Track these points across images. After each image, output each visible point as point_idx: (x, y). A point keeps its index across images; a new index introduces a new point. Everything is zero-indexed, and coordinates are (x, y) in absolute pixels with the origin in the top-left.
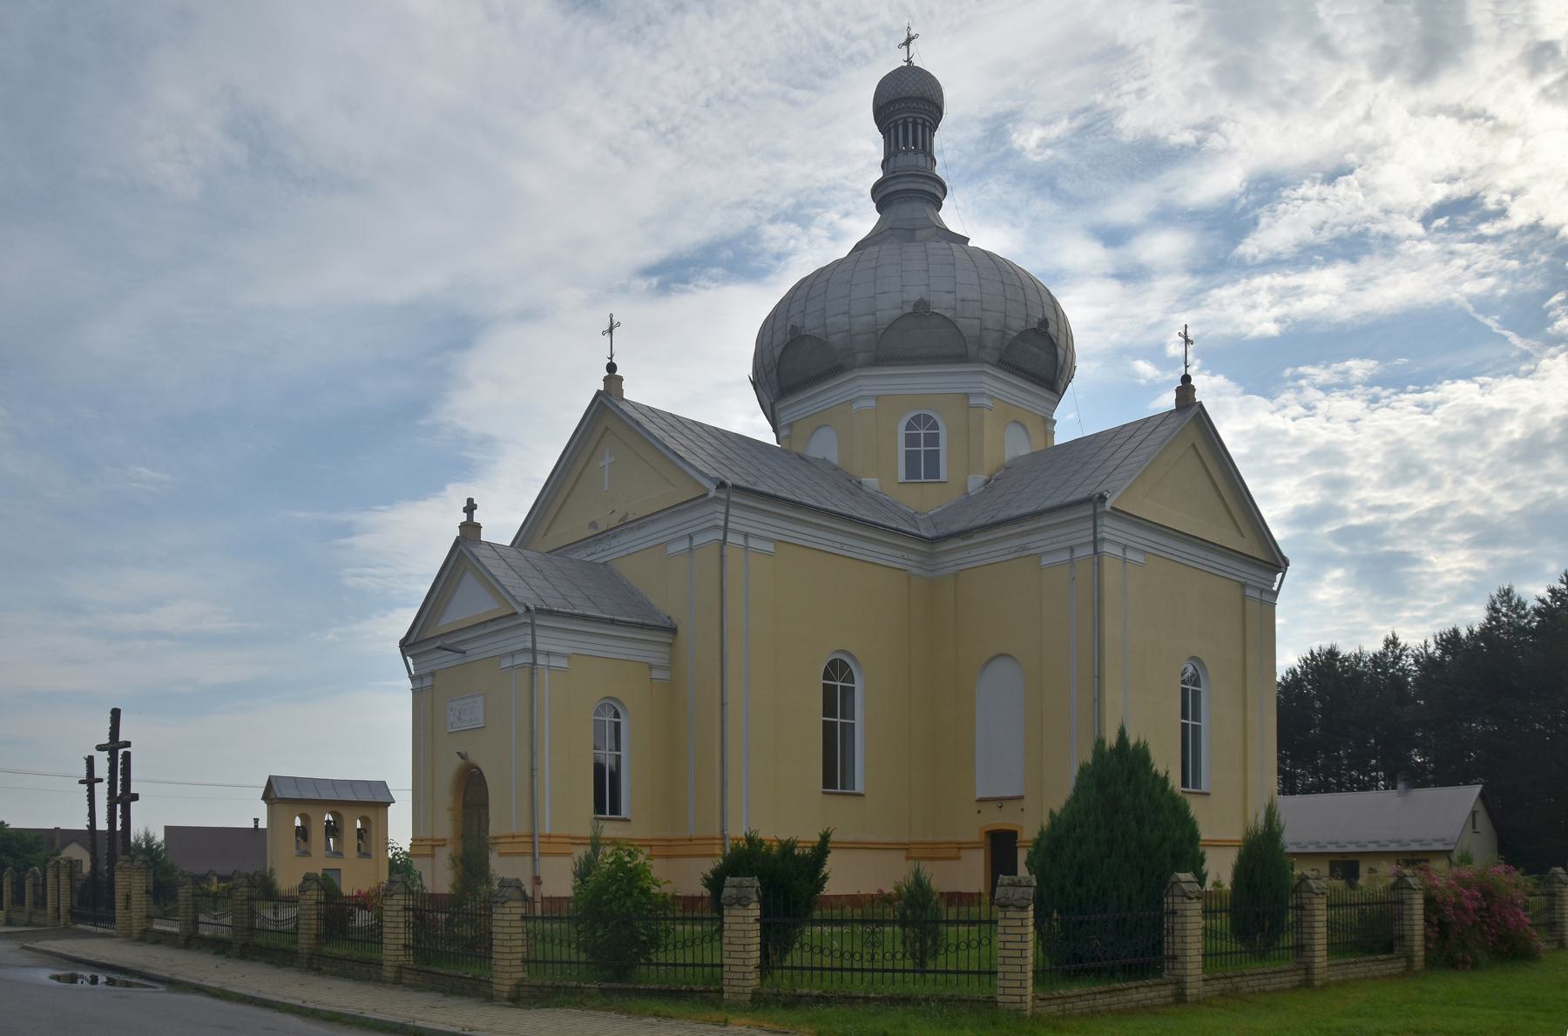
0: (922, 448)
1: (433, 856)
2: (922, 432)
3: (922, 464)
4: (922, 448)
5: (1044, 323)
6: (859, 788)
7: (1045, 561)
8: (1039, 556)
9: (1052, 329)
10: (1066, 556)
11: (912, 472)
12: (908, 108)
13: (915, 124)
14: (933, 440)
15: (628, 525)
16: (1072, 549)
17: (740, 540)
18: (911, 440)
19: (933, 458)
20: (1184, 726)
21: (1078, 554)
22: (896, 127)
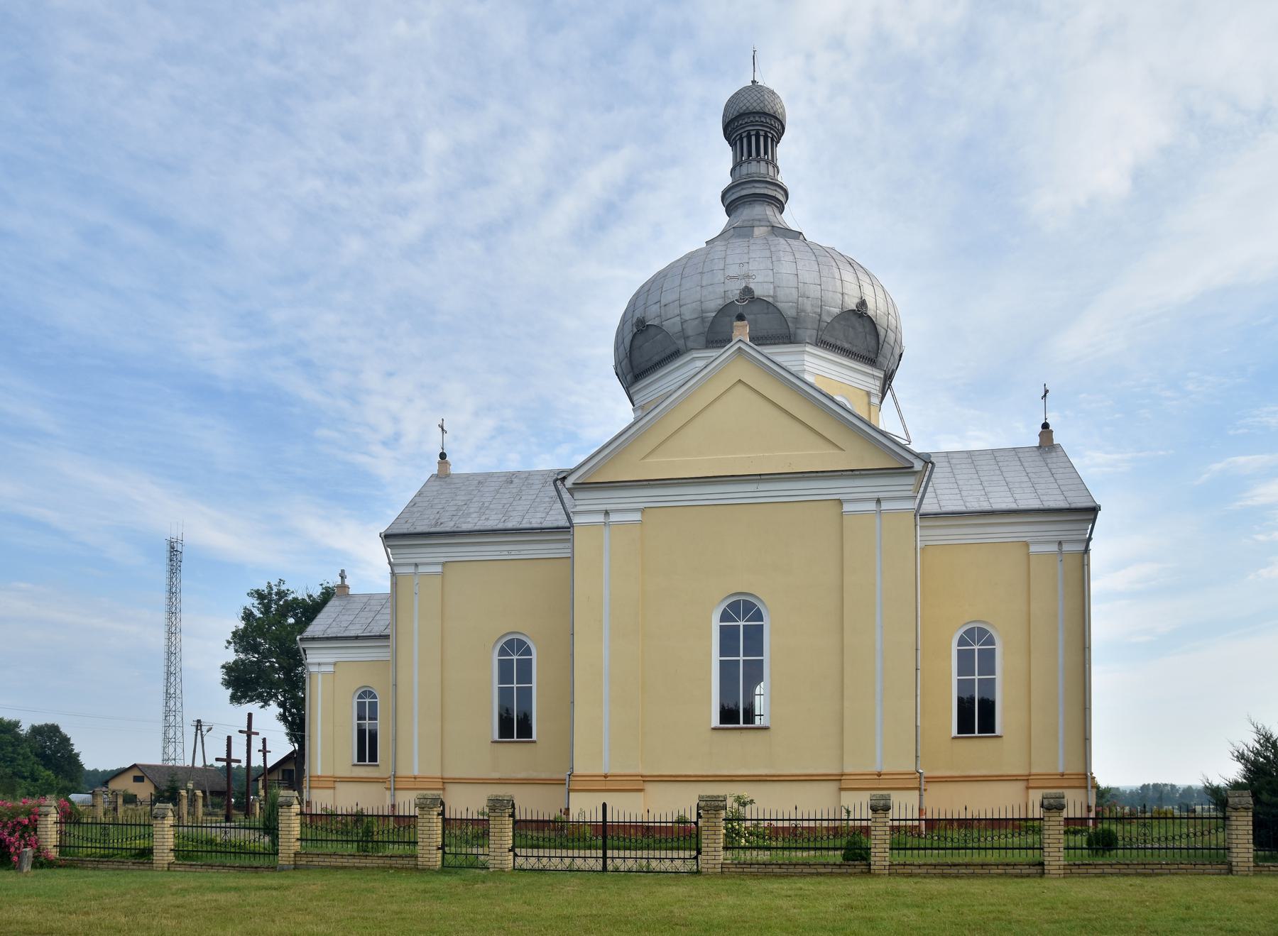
16: (878, 501)
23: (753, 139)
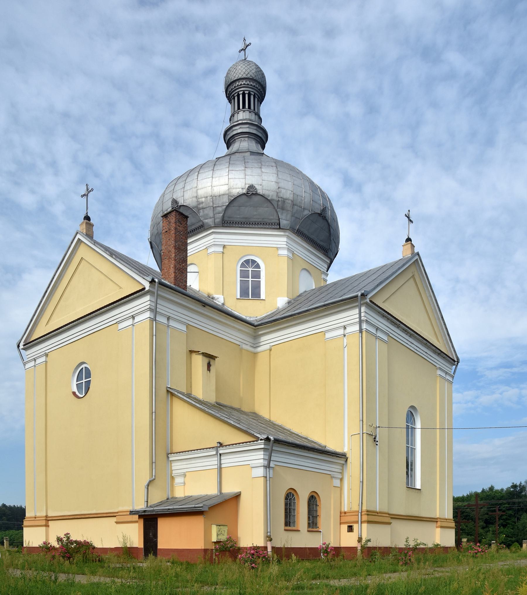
0: (250, 279)
1: (47, 526)
2: (250, 269)
3: (250, 290)
4: (250, 279)
5: (324, 210)
6: (418, 486)
7: (328, 335)
8: (325, 332)
9: (329, 213)
10: (341, 332)
11: (244, 293)
12: (409, 211)
13: (244, 95)
14: (257, 275)
15: (250, 442)
16: (345, 328)
17: (164, 320)
18: (244, 274)
19: (257, 287)
20: (408, 447)
21: (349, 330)
22: (234, 98)
23: (247, 96)
